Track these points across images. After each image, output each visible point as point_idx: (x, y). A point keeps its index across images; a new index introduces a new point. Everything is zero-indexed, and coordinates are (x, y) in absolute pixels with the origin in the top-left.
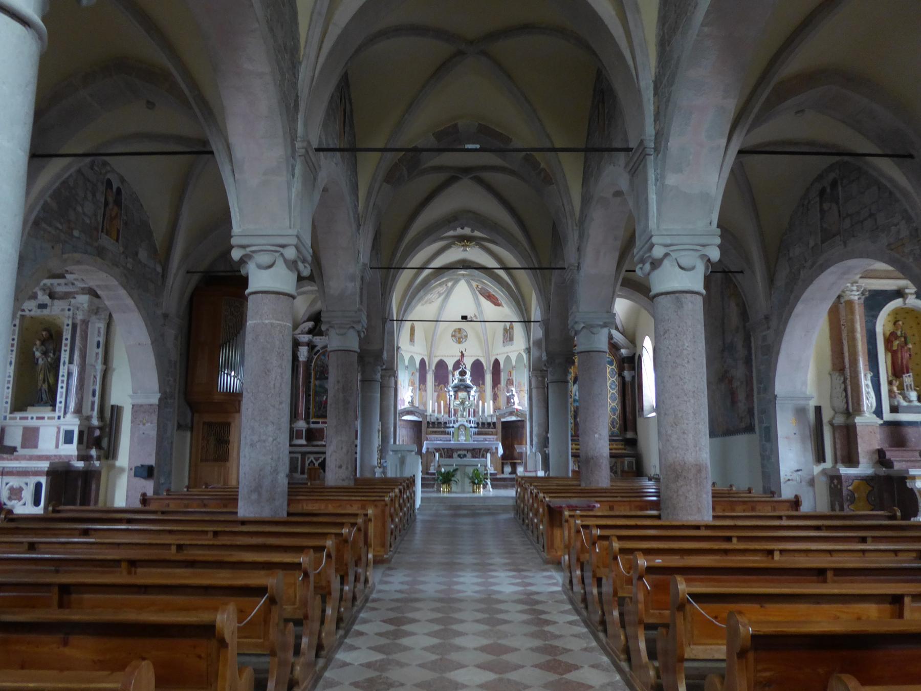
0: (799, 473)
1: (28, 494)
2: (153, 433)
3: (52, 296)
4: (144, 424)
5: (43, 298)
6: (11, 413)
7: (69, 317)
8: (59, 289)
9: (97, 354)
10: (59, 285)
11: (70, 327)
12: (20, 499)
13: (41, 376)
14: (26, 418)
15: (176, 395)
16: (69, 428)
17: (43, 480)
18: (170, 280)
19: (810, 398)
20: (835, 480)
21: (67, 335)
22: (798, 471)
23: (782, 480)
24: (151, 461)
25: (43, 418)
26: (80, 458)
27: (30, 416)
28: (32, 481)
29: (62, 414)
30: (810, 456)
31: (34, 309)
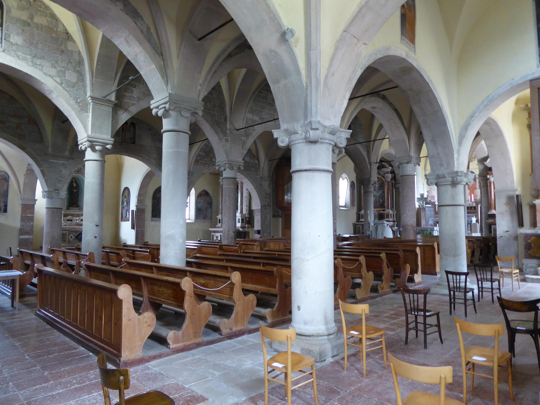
0: (508, 233)
2: (260, 219)
15: (271, 205)
18: (262, 165)
19: (516, 190)
22: (507, 231)
23: (498, 237)
26: (241, 227)
30: (516, 223)
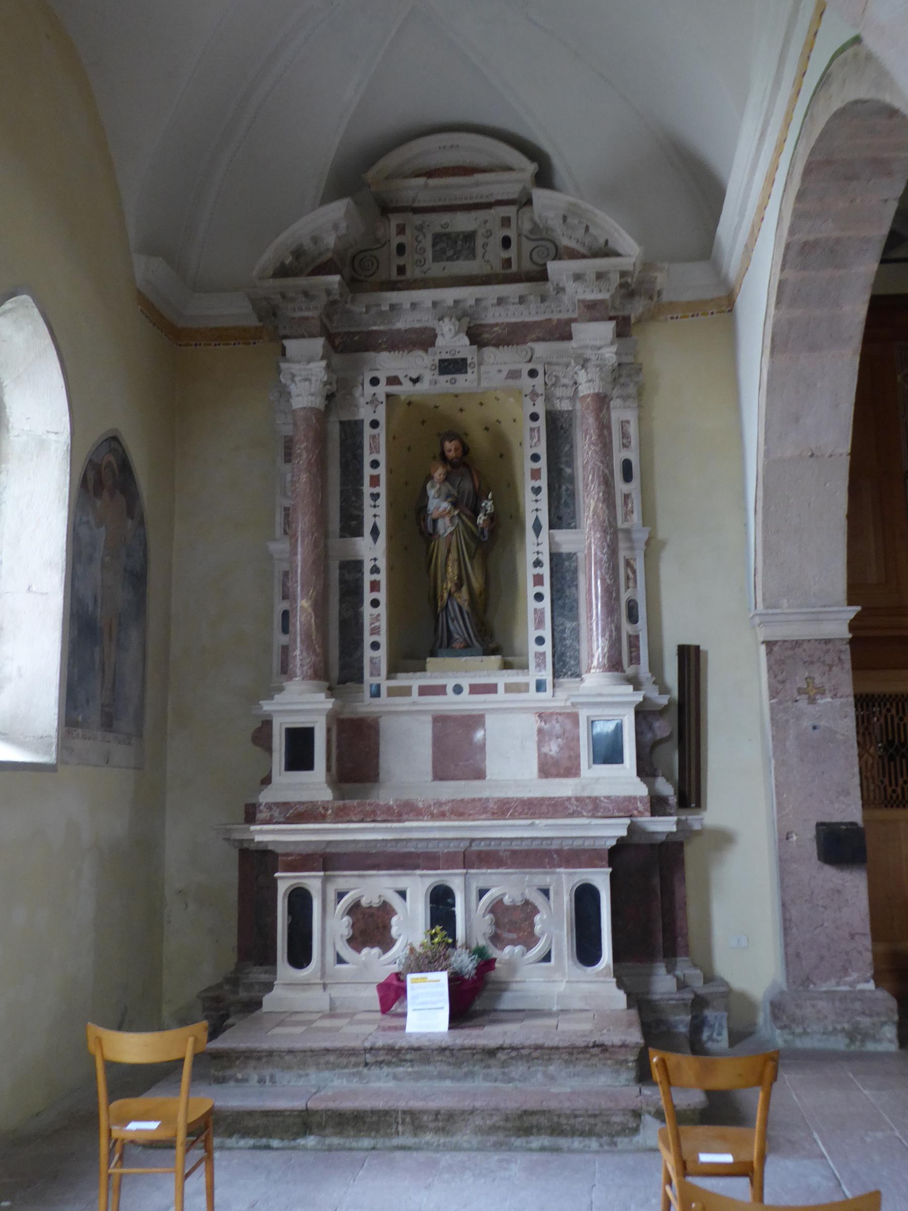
1: (555, 924)
3: (477, 336)
4: (812, 701)
5: (451, 340)
6: (389, 677)
7: (534, 395)
8: (495, 316)
9: (627, 497)
10: (501, 301)
11: (542, 423)
12: (529, 940)
13: (452, 571)
14: (440, 690)
16: (299, 722)
17: (601, 879)
20: (430, 806)
21: (530, 445)
24: (850, 810)
25: (491, 689)
27: (450, 684)
28: (565, 882)
29: (547, 675)
31: (428, 376)
